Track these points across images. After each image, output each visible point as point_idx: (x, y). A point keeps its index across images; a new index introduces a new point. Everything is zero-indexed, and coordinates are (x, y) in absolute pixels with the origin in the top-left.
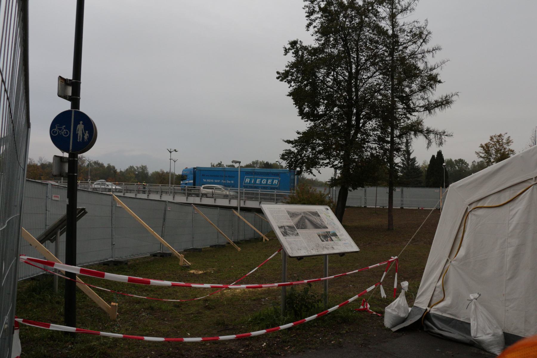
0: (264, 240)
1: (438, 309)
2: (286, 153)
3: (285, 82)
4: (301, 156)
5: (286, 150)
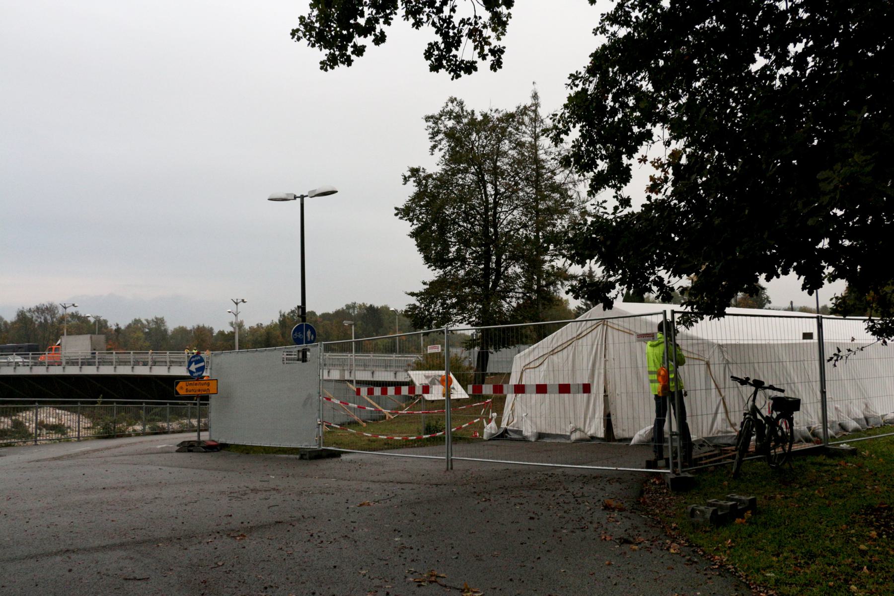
0: (387, 418)
1: (511, 426)
2: (409, 308)
3: (406, 220)
4: (428, 310)
5: (409, 305)
